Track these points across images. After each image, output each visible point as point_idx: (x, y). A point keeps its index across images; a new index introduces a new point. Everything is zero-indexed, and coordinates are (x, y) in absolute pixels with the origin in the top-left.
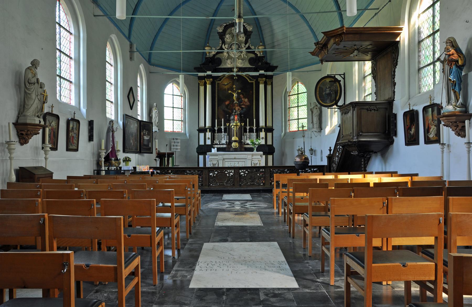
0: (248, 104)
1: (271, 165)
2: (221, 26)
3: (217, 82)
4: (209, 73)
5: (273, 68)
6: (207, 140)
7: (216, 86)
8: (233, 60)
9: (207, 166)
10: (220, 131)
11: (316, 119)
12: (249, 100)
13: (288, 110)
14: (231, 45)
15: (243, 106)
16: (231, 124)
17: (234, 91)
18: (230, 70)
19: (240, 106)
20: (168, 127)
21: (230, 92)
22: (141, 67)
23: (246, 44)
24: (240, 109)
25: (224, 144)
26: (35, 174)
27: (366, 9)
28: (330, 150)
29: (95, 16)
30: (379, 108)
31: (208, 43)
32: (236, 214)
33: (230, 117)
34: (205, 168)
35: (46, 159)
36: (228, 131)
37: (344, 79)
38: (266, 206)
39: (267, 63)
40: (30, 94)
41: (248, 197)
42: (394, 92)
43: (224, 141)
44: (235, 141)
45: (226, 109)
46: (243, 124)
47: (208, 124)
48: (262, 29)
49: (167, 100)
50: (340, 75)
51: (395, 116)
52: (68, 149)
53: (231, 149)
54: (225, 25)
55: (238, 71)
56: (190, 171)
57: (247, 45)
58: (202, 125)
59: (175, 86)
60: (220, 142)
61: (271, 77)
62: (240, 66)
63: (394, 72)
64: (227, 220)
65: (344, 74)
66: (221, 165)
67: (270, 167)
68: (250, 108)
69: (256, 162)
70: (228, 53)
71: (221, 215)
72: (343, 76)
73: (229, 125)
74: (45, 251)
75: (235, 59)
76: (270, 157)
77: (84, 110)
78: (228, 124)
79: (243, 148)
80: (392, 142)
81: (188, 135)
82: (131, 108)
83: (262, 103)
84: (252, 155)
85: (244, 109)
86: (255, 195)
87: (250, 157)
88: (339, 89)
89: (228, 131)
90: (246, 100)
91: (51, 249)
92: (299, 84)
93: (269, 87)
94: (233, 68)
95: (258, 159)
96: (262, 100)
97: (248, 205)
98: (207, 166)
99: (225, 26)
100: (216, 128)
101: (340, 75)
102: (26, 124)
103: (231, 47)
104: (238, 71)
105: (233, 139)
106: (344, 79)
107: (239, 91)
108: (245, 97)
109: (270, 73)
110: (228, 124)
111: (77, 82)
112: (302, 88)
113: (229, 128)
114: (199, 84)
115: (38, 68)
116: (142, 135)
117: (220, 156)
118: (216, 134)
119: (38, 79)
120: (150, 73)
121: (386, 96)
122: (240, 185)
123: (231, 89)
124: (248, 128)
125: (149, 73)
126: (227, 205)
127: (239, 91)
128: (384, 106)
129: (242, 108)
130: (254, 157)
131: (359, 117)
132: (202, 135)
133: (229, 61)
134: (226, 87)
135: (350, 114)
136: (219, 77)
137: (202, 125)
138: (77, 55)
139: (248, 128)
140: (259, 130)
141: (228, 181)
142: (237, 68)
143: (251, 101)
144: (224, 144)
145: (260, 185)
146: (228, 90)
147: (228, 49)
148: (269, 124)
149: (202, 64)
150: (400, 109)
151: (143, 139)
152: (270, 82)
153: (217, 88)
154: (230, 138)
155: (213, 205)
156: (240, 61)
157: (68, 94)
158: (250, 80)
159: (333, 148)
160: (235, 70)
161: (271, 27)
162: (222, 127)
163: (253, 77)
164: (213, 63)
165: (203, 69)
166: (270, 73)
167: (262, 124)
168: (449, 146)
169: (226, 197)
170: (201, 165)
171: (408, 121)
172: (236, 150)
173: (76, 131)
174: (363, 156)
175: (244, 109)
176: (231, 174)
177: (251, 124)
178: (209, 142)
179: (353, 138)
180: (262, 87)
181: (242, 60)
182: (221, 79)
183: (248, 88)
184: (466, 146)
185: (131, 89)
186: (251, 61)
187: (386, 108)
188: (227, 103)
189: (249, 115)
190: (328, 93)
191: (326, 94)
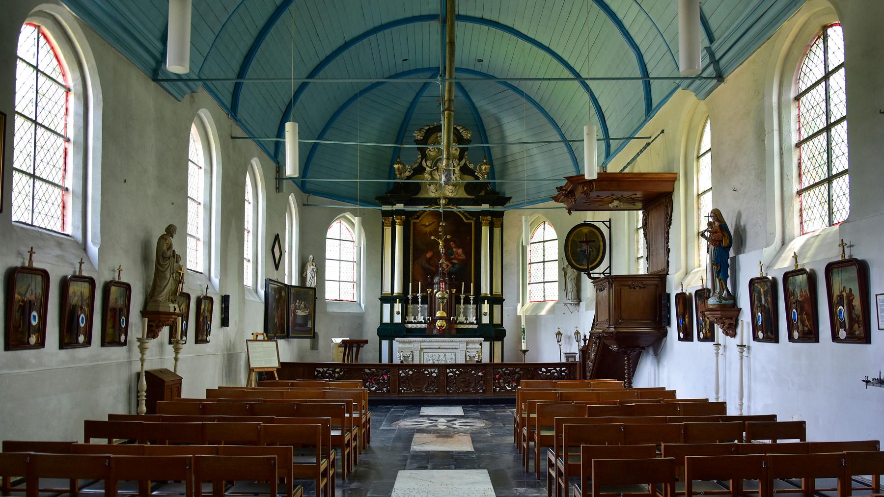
0: (463, 257)
1: (500, 362)
2: (420, 130)
3: (412, 221)
4: (400, 206)
5: (503, 200)
6: (396, 315)
7: (412, 228)
8: (439, 187)
9: (394, 362)
10: (415, 301)
11: (570, 285)
12: (464, 252)
13: (528, 266)
14: (437, 162)
15: (455, 261)
16: (435, 291)
17: (439, 237)
18: (434, 201)
19: (448, 259)
20: (331, 292)
21: (433, 238)
22: (292, 199)
23: (460, 159)
24: (450, 265)
25: (421, 323)
26: (164, 381)
27: (631, 138)
28: (585, 340)
29: (232, 138)
30: (648, 285)
31: (399, 157)
32: (438, 437)
33: (432, 278)
34: (391, 366)
35: (176, 359)
36: (427, 299)
37: (610, 228)
38: (483, 425)
39: (494, 192)
40: (163, 272)
41: (458, 411)
42: (668, 262)
43: (421, 318)
44: (441, 318)
45: (427, 266)
46: (454, 291)
47: (397, 290)
48: (488, 133)
49: (331, 249)
50: (603, 222)
51: (669, 295)
52: (196, 342)
53: (435, 332)
54: (427, 128)
55: (448, 204)
56: (369, 369)
57: (463, 162)
58: (387, 289)
59: (344, 224)
60: (415, 319)
61: (501, 214)
62: (450, 194)
63: (668, 233)
64: (423, 444)
65: (610, 221)
66: (416, 361)
67: (497, 364)
68: (466, 263)
69: (473, 354)
70: (431, 174)
71: (417, 436)
72: (608, 224)
73: (432, 291)
74: (575, 378)
75: (443, 183)
76: (497, 345)
77: (216, 281)
78: (429, 291)
79: (454, 331)
80: (665, 334)
81: (363, 305)
82: (277, 268)
83: (486, 251)
84: (467, 343)
85: (457, 266)
86: (470, 407)
87: (463, 345)
88: (602, 244)
89: (427, 299)
90: (460, 251)
91: (585, 378)
92: (546, 225)
93: (497, 231)
94: (440, 199)
95: (477, 350)
96: (486, 251)
97: (457, 424)
98: (394, 362)
99: (427, 131)
100: (410, 297)
101: (603, 222)
102: (159, 313)
103: (435, 165)
104: (448, 204)
105: (438, 314)
106: (610, 228)
107: (449, 237)
108: (458, 247)
109: (498, 208)
110: (429, 291)
111: (207, 240)
112: (550, 232)
113: (431, 297)
114: (383, 223)
115: (175, 236)
116: (291, 308)
117: (416, 345)
118: (410, 306)
119: (174, 251)
120: (304, 205)
121: (658, 267)
122: (448, 392)
123: (435, 232)
124: (462, 297)
125: (303, 206)
126: (427, 423)
127: (449, 237)
128: (656, 282)
129: (454, 264)
130: (470, 346)
131: (618, 298)
132: (387, 307)
133: (432, 188)
134: (428, 229)
135: (605, 292)
136: (415, 212)
137: (387, 289)
138: (208, 199)
139: (462, 297)
140: (479, 300)
141: (428, 386)
142: (445, 198)
143: (467, 253)
144: (421, 323)
145: (477, 392)
146: (431, 234)
147: (431, 168)
148: (497, 290)
149: (390, 192)
150: (673, 290)
151: (295, 315)
152: (499, 223)
153: (412, 231)
154: (432, 313)
155: (406, 423)
156: (451, 187)
157: (198, 256)
158: (467, 218)
159: (588, 337)
160: (443, 202)
161: (502, 132)
162: (419, 295)
163: (471, 213)
164: (408, 192)
165: (391, 198)
166: (498, 208)
167: (485, 290)
168: (725, 347)
169: (426, 410)
170: (385, 360)
171: (681, 307)
172: (443, 334)
173: (207, 314)
174: (626, 353)
175: (457, 266)
176: (434, 375)
177: (467, 290)
178: (398, 319)
179: (608, 328)
180: (485, 230)
181: (454, 185)
182: (418, 217)
183: (463, 233)
184: (738, 349)
185: (277, 238)
186: (469, 188)
187: (657, 285)
188: (429, 255)
189: (463, 276)
190: (583, 251)
191: (581, 251)
